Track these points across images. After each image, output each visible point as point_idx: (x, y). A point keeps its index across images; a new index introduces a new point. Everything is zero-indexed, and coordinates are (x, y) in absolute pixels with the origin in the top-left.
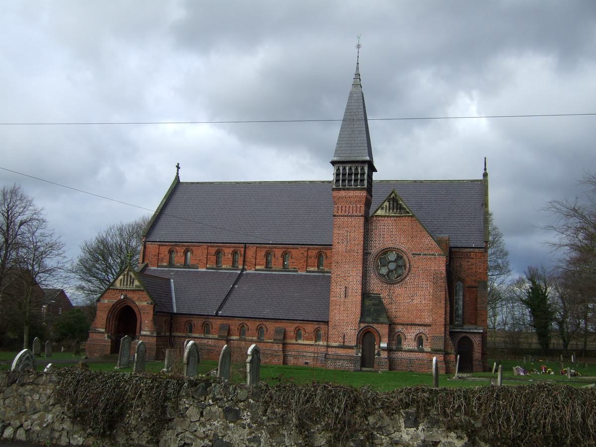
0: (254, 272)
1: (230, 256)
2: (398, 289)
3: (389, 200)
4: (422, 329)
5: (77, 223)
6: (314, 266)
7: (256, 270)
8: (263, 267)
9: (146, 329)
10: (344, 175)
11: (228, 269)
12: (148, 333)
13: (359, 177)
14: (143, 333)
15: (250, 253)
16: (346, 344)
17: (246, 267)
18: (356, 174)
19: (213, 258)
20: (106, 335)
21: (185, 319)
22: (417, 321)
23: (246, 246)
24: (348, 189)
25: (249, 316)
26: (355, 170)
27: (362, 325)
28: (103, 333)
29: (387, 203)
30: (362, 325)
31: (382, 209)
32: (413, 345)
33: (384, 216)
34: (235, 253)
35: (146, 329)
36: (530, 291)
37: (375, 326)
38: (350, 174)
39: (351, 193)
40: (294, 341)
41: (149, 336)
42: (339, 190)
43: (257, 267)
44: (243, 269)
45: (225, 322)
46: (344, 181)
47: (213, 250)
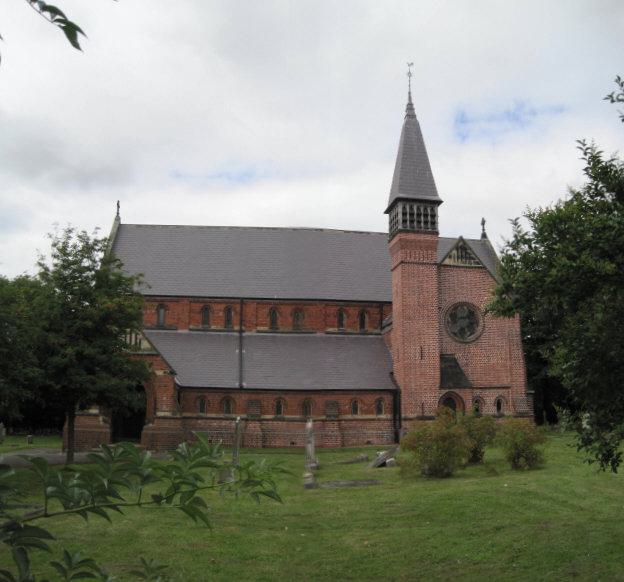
0: (255, 334)
1: (221, 314)
2: (473, 348)
3: (457, 248)
4: (501, 392)
5: (11, 275)
6: (333, 326)
7: (258, 332)
8: (266, 328)
9: (164, 408)
10: (412, 215)
11: (220, 331)
12: (167, 414)
13: (408, 216)
14: (160, 414)
15: (250, 309)
16: (425, 414)
17: (243, 328)
18: (426, 216)
19: (199, 317)
20: (101, 419)
21: (194, 395)
22: (496, 384)
23: (243, 301)
24: (418, 232)
25: (492, 391)
26: (415, 207)
27: (444, 392)
28: (95, 415)
29: (455, 252)
30: (444, 392)
31: (450, 257)
32: (493, 410)
33: (454, 266)
34: (228, 311)
35: (164, 408)
36: (115, 329)
37: (457, 391)
38: (419, 215)
39: (422, 237)
40: (349, 417)
41: (171, 418)
42: (408, 232)
43: (259, 328)
44: (241, 331)
45: (254, 397)
46: (412, 222)
47: (197, 307)
